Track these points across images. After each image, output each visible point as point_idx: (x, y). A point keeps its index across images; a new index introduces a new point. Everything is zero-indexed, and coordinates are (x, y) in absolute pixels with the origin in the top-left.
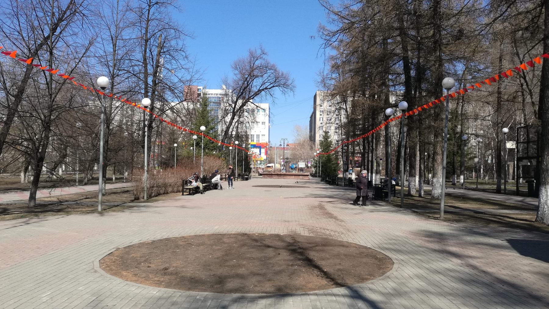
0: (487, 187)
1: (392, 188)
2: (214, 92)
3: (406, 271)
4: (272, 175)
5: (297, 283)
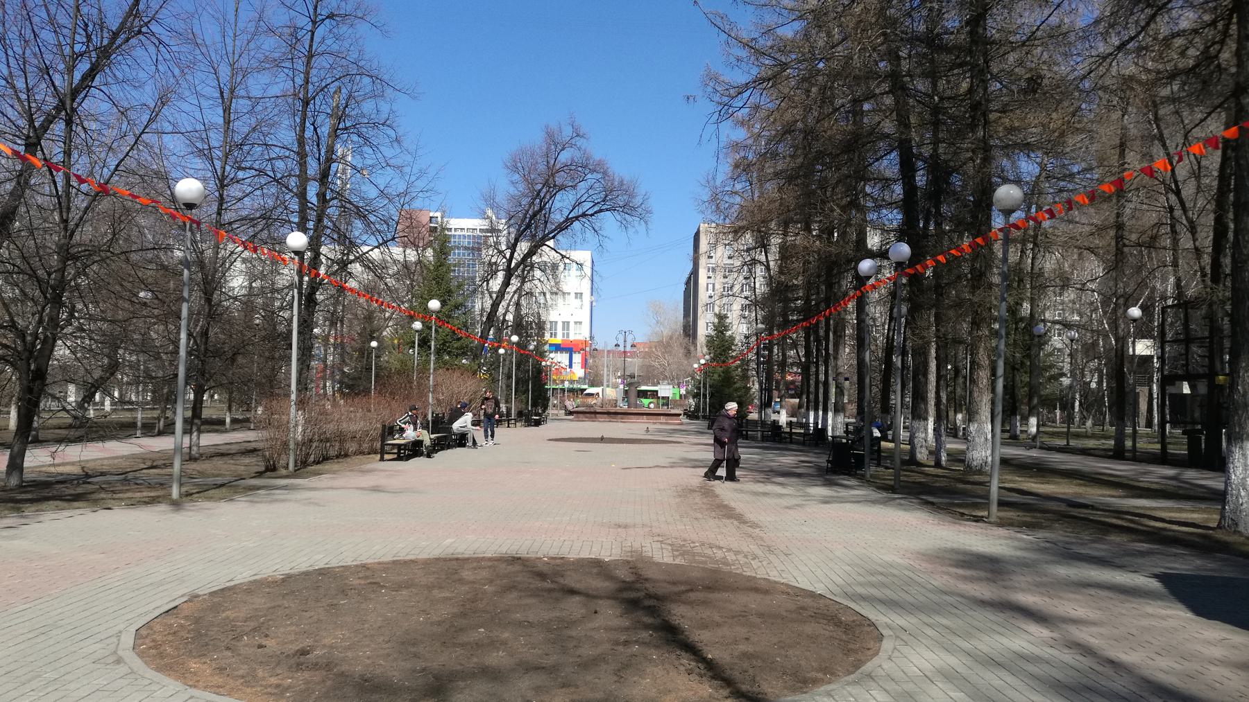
0: (1091, 443)
1: (872, 445)
2: (464, 225)
3: (915, 659)
4: (596, 413)
5: (634, 692)
